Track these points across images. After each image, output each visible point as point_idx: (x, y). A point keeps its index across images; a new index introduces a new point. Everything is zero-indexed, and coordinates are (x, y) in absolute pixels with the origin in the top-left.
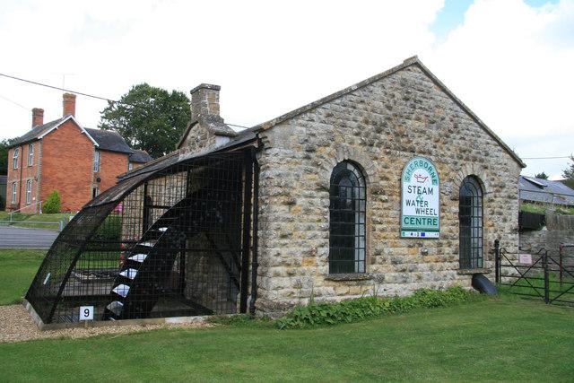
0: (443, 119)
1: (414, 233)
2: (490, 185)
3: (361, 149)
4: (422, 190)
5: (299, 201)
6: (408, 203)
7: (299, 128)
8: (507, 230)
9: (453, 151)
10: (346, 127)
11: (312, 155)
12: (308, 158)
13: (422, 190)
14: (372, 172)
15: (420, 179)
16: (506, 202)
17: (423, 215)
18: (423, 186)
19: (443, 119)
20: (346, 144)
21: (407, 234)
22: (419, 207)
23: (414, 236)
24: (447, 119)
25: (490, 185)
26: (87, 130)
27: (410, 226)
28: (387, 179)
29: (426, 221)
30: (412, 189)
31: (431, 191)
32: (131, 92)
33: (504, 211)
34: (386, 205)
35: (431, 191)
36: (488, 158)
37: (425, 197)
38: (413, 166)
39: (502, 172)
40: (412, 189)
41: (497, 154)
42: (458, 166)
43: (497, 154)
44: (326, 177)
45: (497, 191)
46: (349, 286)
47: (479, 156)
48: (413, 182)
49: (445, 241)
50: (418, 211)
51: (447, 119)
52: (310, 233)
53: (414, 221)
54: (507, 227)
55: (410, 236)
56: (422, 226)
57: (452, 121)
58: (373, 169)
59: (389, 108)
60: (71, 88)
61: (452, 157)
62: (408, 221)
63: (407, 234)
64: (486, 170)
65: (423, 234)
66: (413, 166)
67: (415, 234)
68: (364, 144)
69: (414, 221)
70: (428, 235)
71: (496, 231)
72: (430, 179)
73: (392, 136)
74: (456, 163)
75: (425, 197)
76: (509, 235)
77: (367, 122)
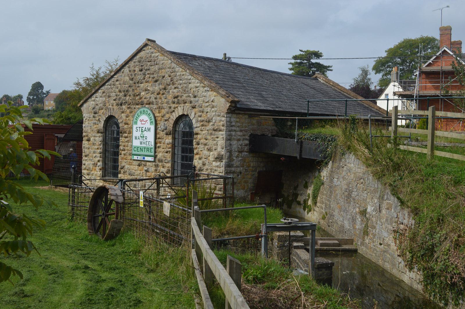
0: (164, 77)
1: (139, 157)
2: (197, 121)
3: (115, 107)
4: (144, 129)
5: (92, 139)
6: (136, 138)
7: (92, 102)
8: (211, 158)
9: (170, 97)
10: (111, 97)
11: (96, 115)
12: (94, 117)
13: (144, 129)
14: (121, 120)
15: (143, 122)
16: (211, 134)
17: (144, 145)
18: (144, 126)
19: (164, 77)
20: (111, 107)
21: (135, 158)
22: (142, 140)
23: (138, 159)
24: (167, 76)
25: (197, 121)
26: (225, 266)
27: (136, 153)
28: (128, 124)
29: (146, 149)
30: (138, 129)
31: (149, 130)
32: (400, 44)
33: (210, 143)
34: (126, 139)
35: (149, 130)
36: (197, 99)
37: (146, 134)
38: (139, 114)
39: (209, 109)
40: (138, 129)
41: (205, 94)
42: (173, 109)
43: (205, 94)
44: (101, 125)
45: (203, 125)
46: (109, 184)
47: (189, 98)
48: (139, 124)
49: (160, 164)
50: (141, 143)
51: (167, 76)
52: (94, 155)
53: (139, 150)
54: (213, 155)
55: (136, 159)
56: (143, 153)
57: (170, 76)
58: (121, 118)
59: (132, 79)
60: (333, 71)
61: (167, 103)
62: (136, 149)
63: (135, 158)
64: (195, 109)
65: (144, 158)
66: (139, 114)
67: (140, 158)
68: (117, 105)
69: (139, 150)
70: (147, 159)
71: (200, 159)
72: (149, 121)
73: (132, 97)
74: (170, 108)
75: (146, 134)
76: (214, 163)
77: (120, 91)
